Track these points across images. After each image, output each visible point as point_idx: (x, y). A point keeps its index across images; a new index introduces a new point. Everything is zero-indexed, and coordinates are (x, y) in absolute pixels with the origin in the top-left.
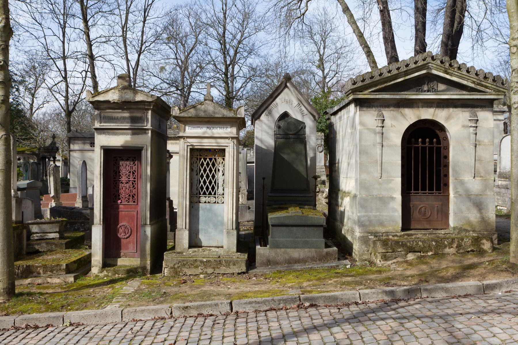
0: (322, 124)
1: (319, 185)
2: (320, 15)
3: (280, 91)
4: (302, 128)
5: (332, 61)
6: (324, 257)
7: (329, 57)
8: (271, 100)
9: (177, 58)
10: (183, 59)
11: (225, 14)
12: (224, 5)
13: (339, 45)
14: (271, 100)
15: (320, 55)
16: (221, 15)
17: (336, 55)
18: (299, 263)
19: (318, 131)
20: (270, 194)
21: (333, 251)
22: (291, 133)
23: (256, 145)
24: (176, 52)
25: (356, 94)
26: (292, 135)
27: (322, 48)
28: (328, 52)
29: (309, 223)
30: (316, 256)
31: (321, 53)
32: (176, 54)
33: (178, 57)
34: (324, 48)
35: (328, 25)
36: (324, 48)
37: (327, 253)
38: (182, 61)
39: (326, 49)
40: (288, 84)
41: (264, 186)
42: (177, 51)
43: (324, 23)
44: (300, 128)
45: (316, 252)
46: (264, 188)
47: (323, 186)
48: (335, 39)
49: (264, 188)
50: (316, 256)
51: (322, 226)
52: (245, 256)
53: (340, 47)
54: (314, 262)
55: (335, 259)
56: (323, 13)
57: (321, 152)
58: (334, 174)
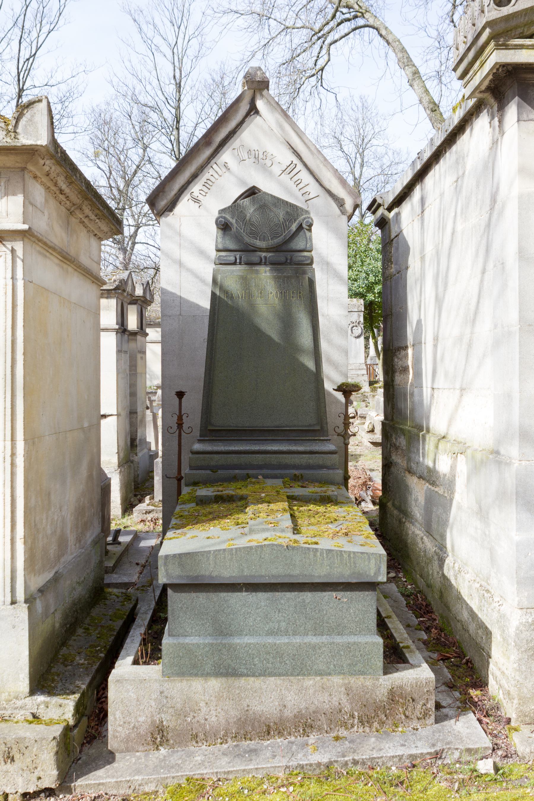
0: (360, 282)
1: (355, 403)
2: (355, 108)
3: (232, 124)
4: (300, 228)
5: (375, 189)
6: (379, 708)
7: (371, 181)
8: (208, 152)
9: (111, 187)
10: (121, 188)
11: (179, 86)
12: (177, 71)
13: (386, 161)
14: (208, 152)
15: (355, 179)
16: (171, 89)
17: (382, 178)
18: (280, 734)
19: (350, 296)
20: (197, 447)
21: (418, 685)
22: (262, 244)
23: (164, 292)
24: (108, 174)
25: (507, 47)
26: (267, 250)
27: (358, 166)
28: (368, 172)
29: (320, 573)
30: (347, 708)
31: (357, 175)
32: (108, 178)
33: (113, 185)
34: (362, 166)
35: (368, 127)
36: (362, 166)
37: (395, 696)
38: (119, 190)
39: (365, 169)
40: (260, 104)
41: (180, 418)
42: (111, 173)
43: (361, 122)
44: (294, 227)
45: (348, 690)
46: (180, 425)
47: (363, 404)
48: (381, 150)
49: (180, 425)
50: (347, 708)
51: (370, 586)
52: (62, 709)
53: (388, 164)
54: (343, 732)
55: (425, 715)
56: (360, 105)
57: (359, 337)
58: (398, 378)
